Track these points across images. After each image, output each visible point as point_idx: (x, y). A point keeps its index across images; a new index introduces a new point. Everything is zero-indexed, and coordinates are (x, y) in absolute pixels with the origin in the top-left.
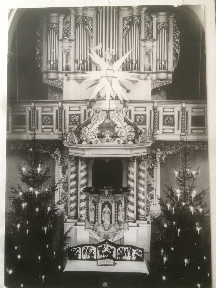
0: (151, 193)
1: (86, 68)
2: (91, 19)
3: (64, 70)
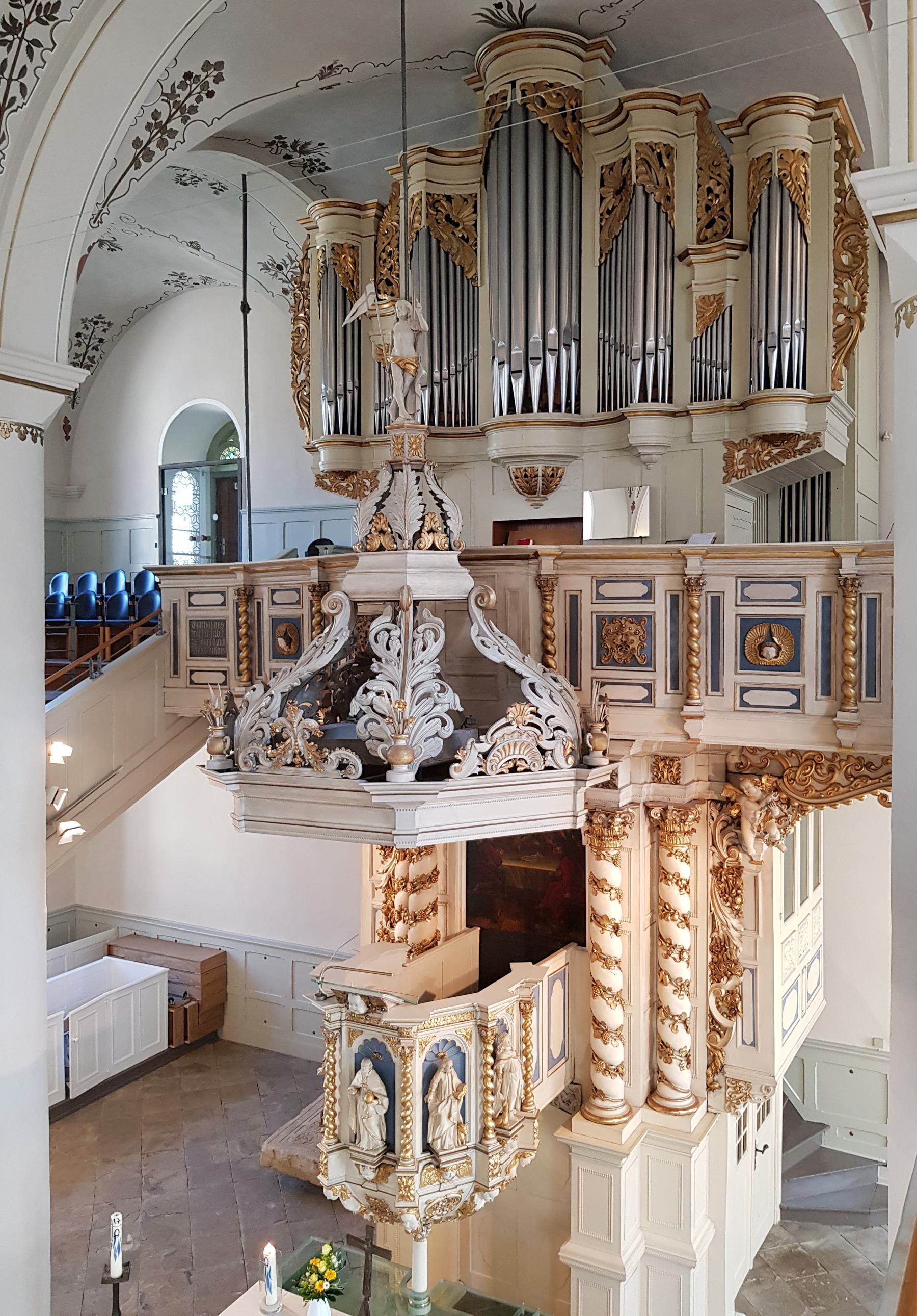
0: (727, 985)
1: (463, 413)
2: (471, 200)
3: (380, 432)
